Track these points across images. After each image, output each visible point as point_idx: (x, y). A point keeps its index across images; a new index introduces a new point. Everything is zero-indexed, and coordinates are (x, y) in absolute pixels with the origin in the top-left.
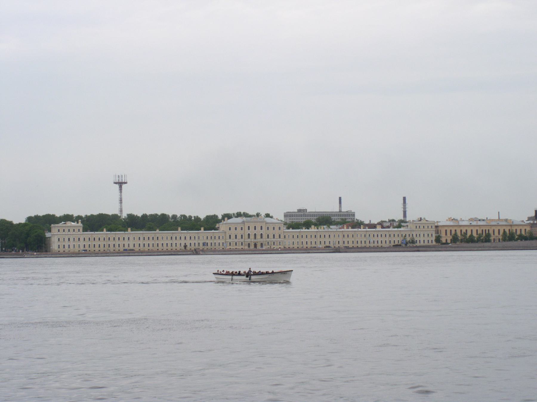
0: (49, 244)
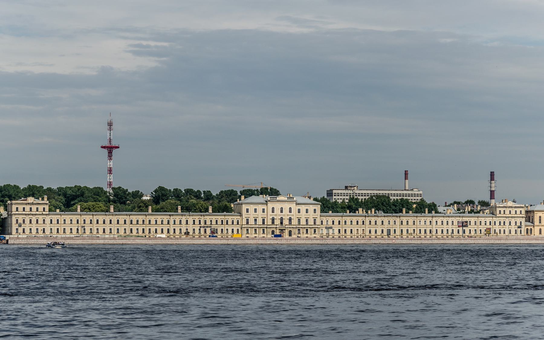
0: (5, 227)
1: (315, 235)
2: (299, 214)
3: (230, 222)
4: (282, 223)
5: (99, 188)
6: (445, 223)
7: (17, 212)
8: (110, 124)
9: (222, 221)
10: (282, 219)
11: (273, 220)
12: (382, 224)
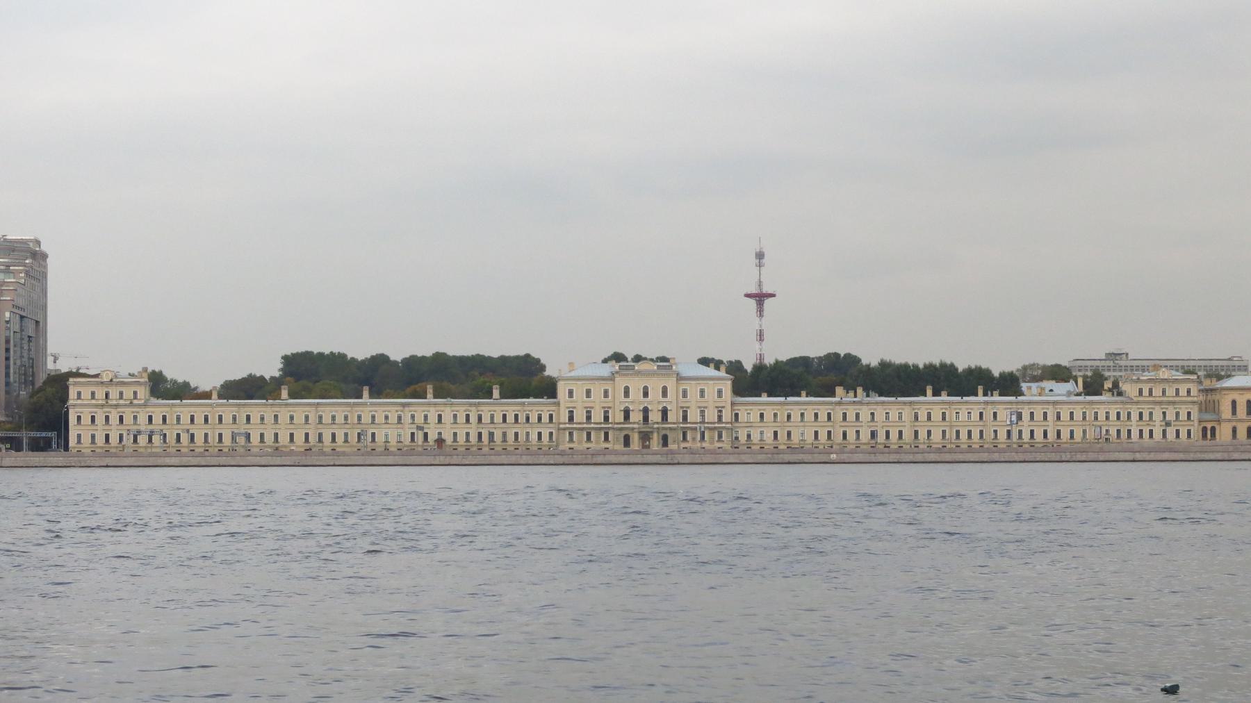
1: (589, 445)
2: (702, 399)
3: (533, 419)
4: (646, 419)
7: (79, 402)
8: (760, 256)
9: (516, 416)
11: (627, 413)
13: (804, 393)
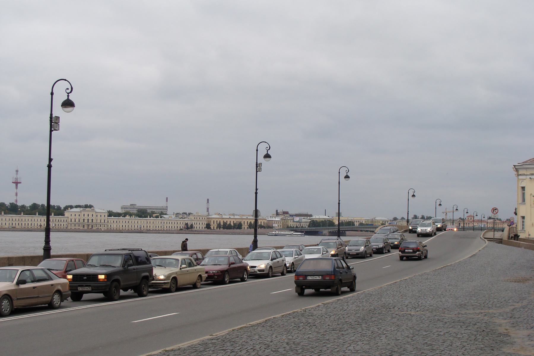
3: (62, 221)
5: (3, 203)
6: (168, 223)
8: (17, 171)
10: (88, 219)
11: (84, 220)
12: (41, 221)
13: (121, 216)
